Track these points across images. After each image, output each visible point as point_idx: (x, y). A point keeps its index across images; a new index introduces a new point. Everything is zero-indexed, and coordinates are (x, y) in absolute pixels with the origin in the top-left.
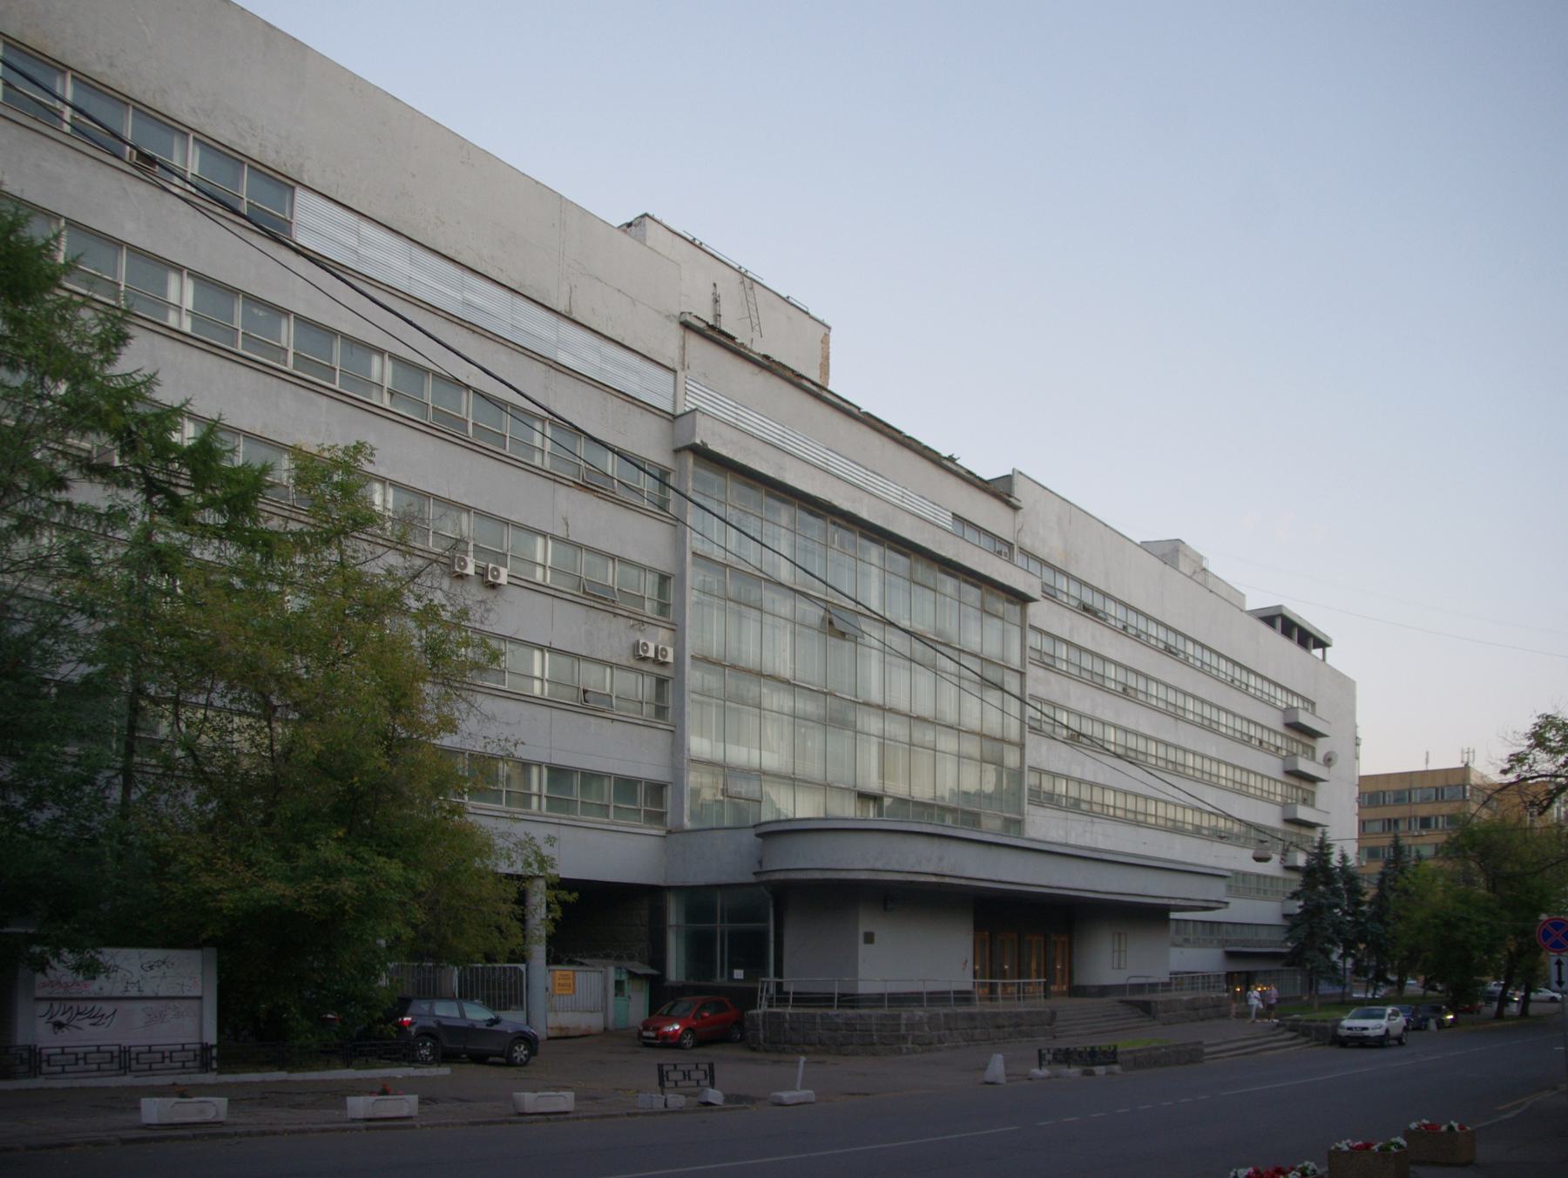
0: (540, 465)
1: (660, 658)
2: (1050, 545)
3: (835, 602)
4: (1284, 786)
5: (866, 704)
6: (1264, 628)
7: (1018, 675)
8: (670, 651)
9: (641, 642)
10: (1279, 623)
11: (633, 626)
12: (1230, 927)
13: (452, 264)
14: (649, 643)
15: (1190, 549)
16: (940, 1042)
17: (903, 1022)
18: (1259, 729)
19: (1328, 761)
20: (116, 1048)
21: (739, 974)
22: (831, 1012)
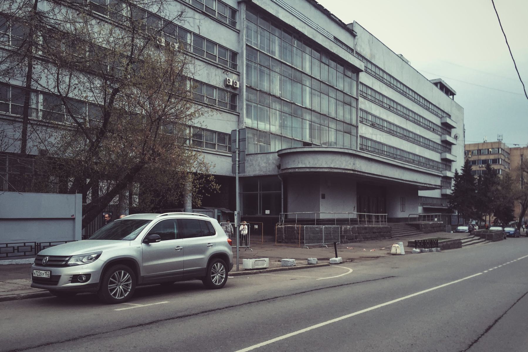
0: (188, 2)
1: (234, 86)
2: (365, 51)
3: (295, 67)
4: (441, 146)
5: (306, 108)
6: (434, 87)
7: (356, 100)
10: (439, 86)
11: (224, 72)
12: (425, 199)
13: (275, 4)
14: (230, 79)
15: (404, 58)
18: (433, 125)
19: (456, 137)
20: (33, 244)
21: (267, 212)
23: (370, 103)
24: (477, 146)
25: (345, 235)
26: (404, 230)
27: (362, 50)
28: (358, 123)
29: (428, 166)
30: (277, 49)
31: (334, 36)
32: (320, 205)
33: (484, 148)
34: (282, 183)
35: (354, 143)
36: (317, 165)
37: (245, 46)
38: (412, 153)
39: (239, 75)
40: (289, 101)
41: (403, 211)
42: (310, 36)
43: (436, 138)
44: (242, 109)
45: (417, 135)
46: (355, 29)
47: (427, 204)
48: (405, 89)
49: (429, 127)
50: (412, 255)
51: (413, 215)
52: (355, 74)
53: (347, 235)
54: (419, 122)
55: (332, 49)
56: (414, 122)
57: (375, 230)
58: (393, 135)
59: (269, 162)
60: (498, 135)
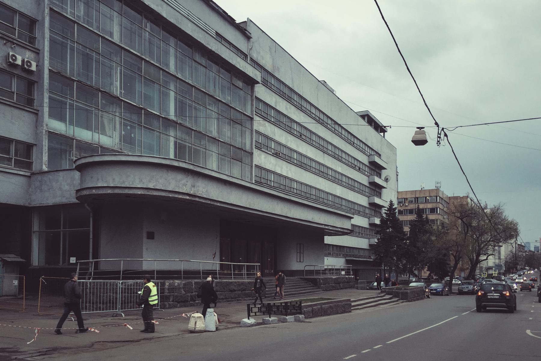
8: (34, 64)
9: (11, 53)
11: (5, 44)
14: (17, 56)
19: (386, 180)
23: (273, 126)
24: (414, 193)
25: (170, 296)
27: (259, 58)
28: (253, 150)
29: (352, 211)
30: (116, 30)
31: (216, 32)
32: (144, 248)
33: (421, 196)
34: (91, 215)
35: (248, 174)
37: (47, 11)
38: (331, 194)
39: (38, 54)
40: (135, 104)
41: (300, 262)
42: (172, 21)
43: (364, 179)
44: (42, 105)
45: (339, 173)
46: (249, 29)
47: (350, 256)
48: (322, 116)
49: (353, 165)
50: (241, 329)
51: (217, 174)
52: (250, 87)
53: (174, 295)
54: (340, 158)
55: (209, 45)
56: (334, 158)
57: (232, 287)
58: (306, 170)
59: (74, 182)
60: (436, 182)
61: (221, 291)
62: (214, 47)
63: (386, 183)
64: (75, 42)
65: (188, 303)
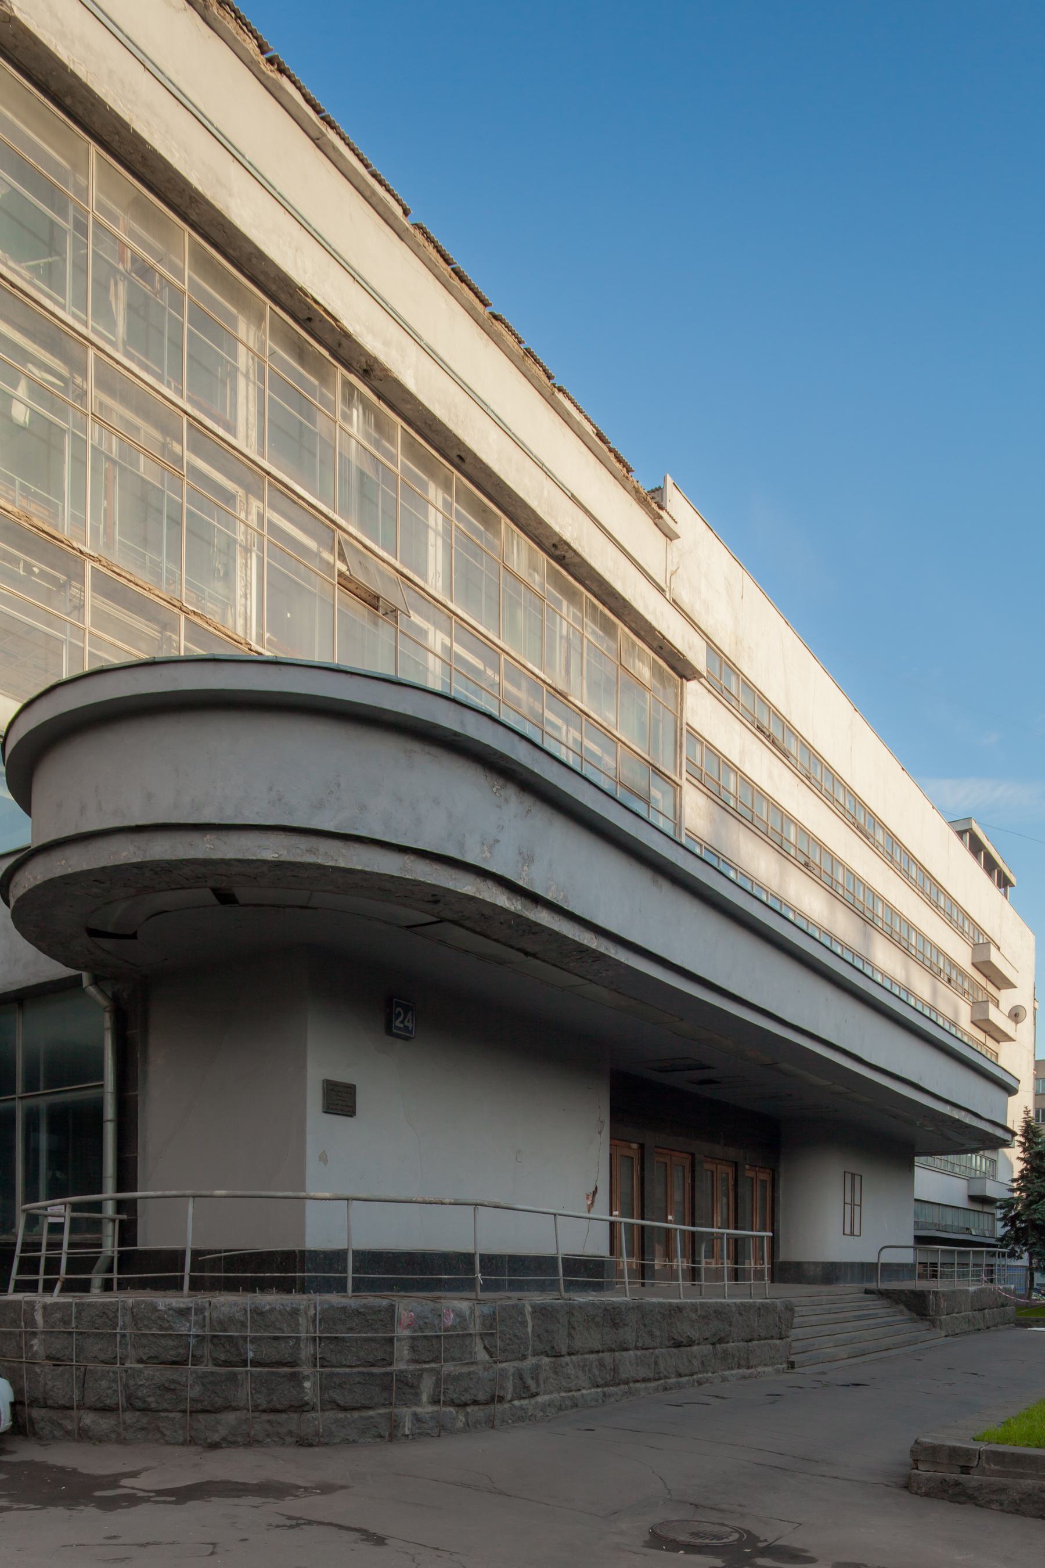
16: (525, 1392)
17: (402, 1332)
22: (165, 1301)
26: (859, 1318)
36: (303, 847)
41: (852, 1234)
57: (685, 1329)
61: (640, 1344)
62: (570, 527)
63: (1013, 1024)
64: (86, 415)
65: (506, 1406)
